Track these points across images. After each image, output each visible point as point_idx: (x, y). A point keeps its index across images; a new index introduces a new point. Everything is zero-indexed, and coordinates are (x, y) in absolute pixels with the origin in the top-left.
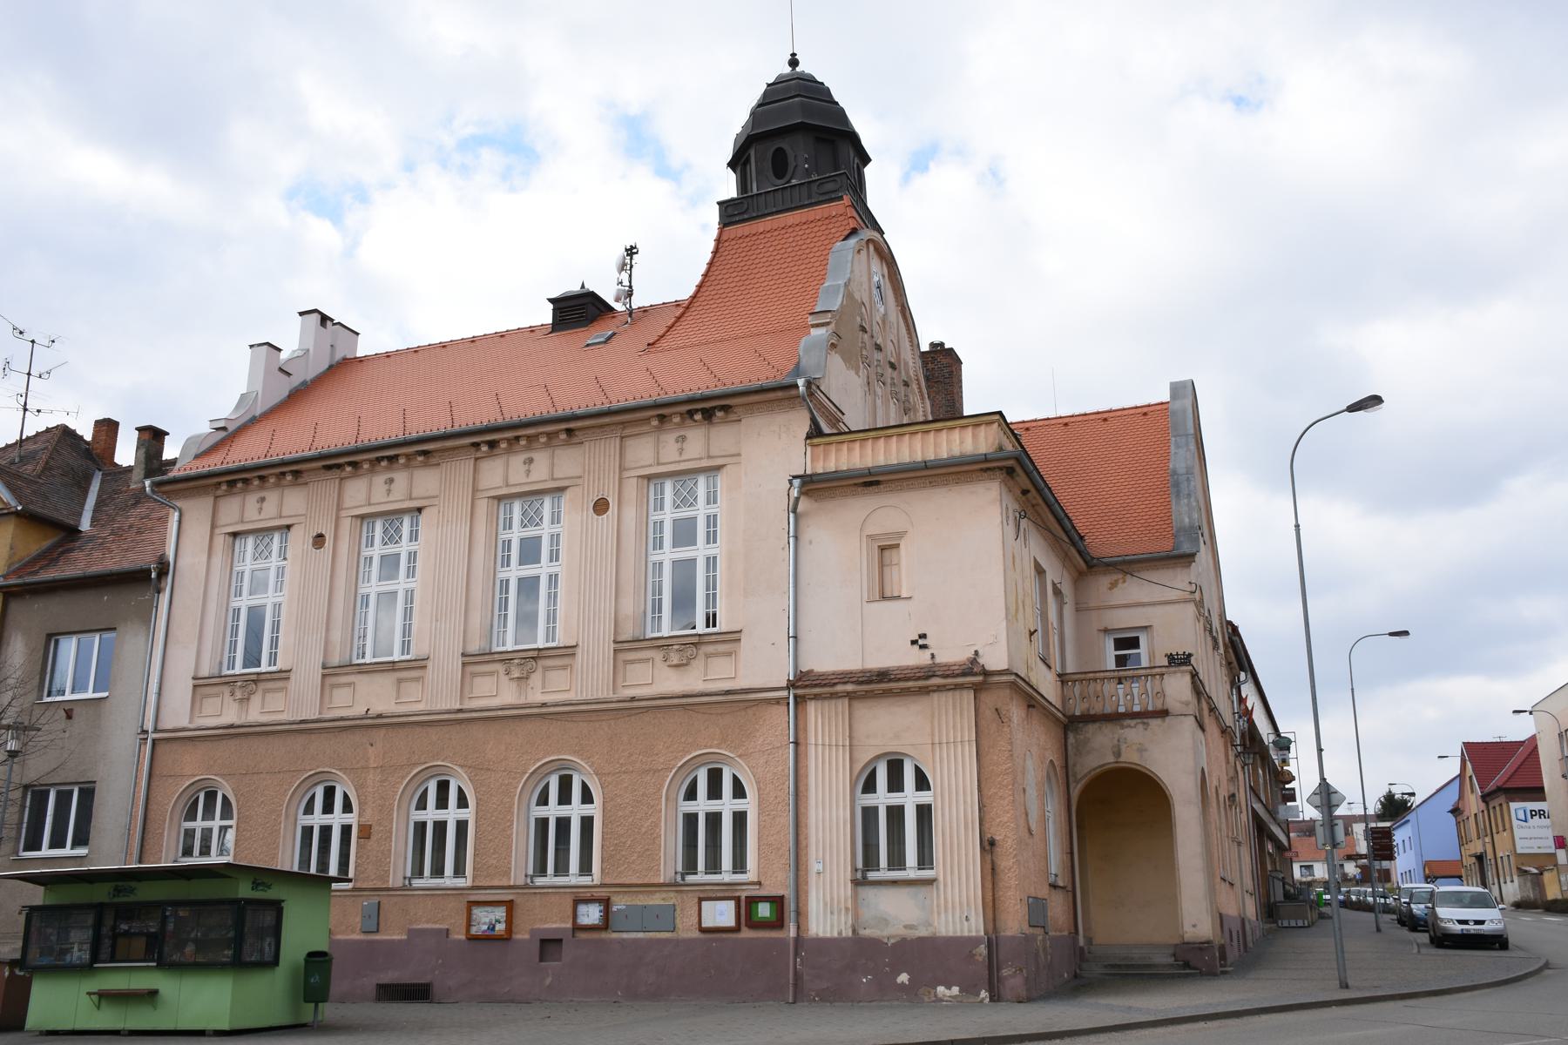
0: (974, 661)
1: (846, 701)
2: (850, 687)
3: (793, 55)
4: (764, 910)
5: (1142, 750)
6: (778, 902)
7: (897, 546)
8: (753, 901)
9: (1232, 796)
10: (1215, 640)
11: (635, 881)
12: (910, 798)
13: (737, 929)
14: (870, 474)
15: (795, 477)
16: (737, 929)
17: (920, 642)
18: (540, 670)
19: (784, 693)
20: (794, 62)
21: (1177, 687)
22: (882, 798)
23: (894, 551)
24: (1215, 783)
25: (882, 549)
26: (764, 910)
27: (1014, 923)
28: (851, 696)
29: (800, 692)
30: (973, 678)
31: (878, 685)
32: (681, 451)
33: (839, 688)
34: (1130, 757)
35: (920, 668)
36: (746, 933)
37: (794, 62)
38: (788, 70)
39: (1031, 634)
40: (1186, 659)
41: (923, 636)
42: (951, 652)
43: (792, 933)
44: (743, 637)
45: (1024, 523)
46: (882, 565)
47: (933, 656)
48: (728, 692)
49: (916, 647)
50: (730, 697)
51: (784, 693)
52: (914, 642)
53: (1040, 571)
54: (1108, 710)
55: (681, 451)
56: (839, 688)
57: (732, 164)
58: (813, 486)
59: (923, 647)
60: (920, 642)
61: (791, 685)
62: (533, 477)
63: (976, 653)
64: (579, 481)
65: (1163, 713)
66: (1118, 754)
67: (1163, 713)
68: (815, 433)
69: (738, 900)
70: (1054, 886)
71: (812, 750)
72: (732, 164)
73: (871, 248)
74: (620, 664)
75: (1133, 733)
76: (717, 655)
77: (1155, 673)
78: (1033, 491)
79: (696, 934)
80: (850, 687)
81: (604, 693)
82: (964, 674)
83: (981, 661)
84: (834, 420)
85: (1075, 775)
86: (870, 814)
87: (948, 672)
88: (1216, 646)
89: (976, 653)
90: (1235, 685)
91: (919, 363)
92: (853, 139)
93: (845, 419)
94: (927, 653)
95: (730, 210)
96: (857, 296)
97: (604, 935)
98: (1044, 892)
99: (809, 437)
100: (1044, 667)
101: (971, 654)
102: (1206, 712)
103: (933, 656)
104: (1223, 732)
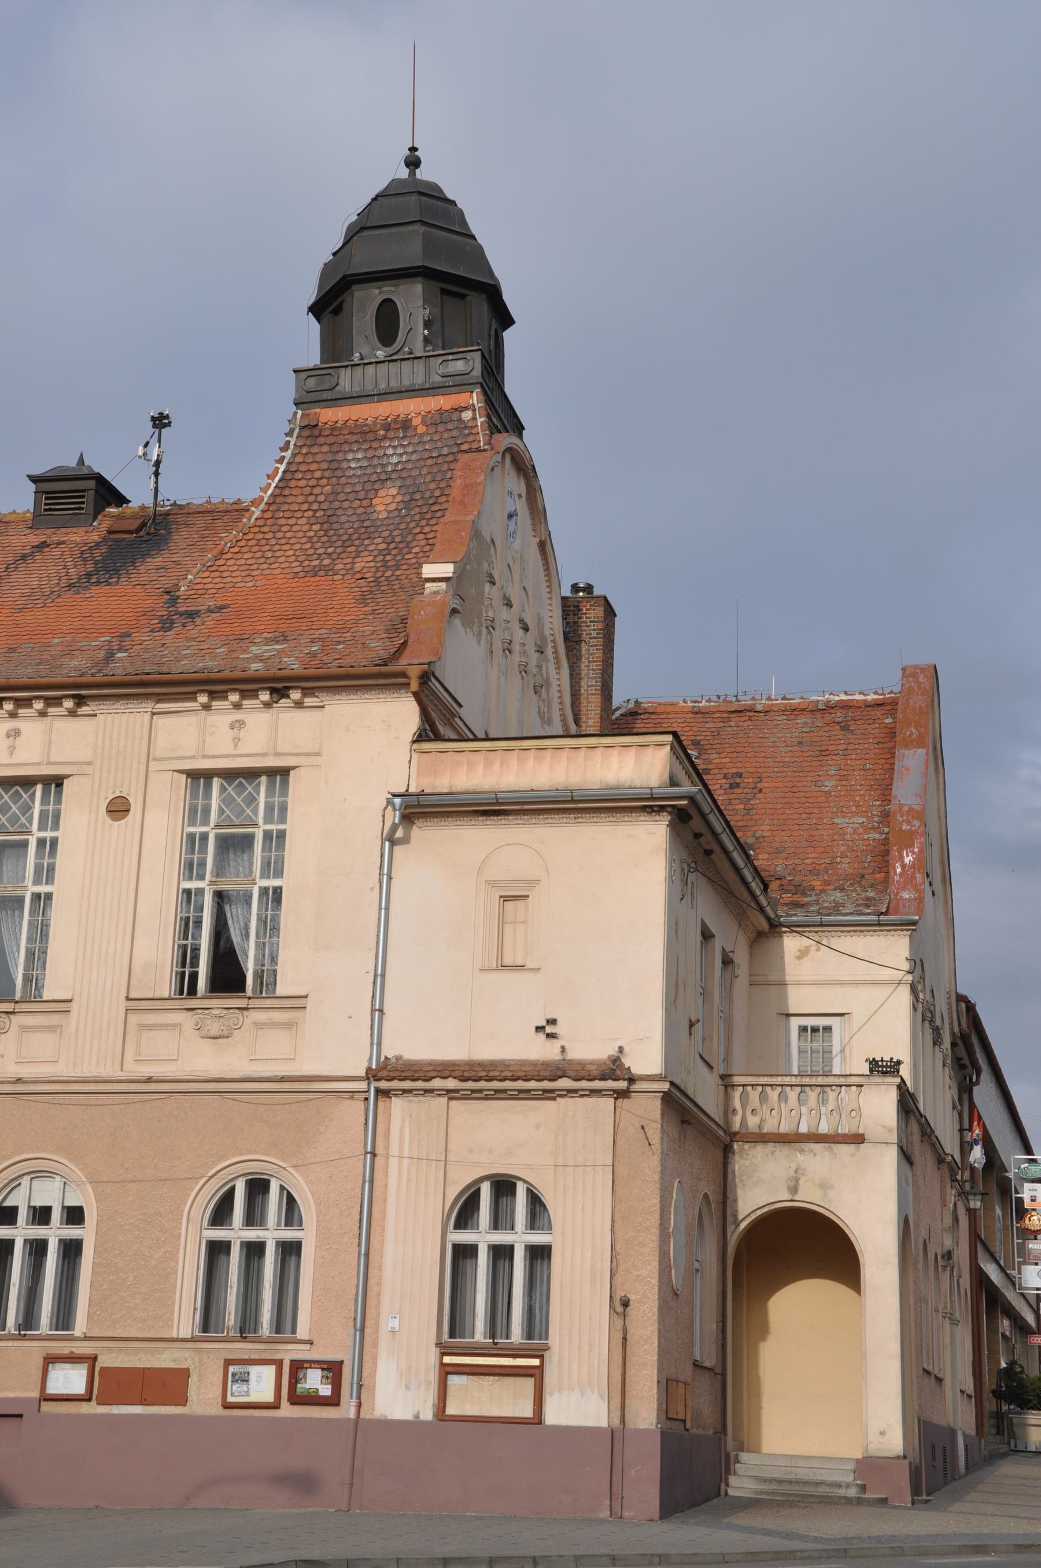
0: (616, 1060)
1: (445, 1100)
2: (451, 1083)
3: (413, 149)
4: (314, 1381)
5: (825, 1186)
6: (333, 1370)
7: (528, 896)
8: (298, 1367)
9: (948, 1255)
10: (937, 1031)
11: (133, 1334)
12: (272, 1233)
13: (275, 1406)
14: (498, 803)
15: (395, 796)
16: (275, 1406)
17: (547, 1029)
18: (14, 1030)
19: (362, 1086)
20: (413, 162)
21: (879, 1107)
22: (237, 1232)
23: (520, 904)
24: (923, 1234)
25: (506, 899)
26: (314, 1381)
27: (646, 1415)
28: (451, 1094)
29: (383, 1085)
30: (613, 1077)
31: (480, 1081)
32: (236, 741)
33: (437, 1083)
34: (809, 1197)
35: (546, 1064)
36: (287, 1410)
37: (413, 162)
38: (404, 173)
39: (691, 1025)
40: (891, 1068)
41: (552, 1022)
42: (588, 1047)
43: (352, 1415)
44: (309, 1003)
45: (692, 877)
46: (502, 922)
47: (563, 1049)
48: (283, 1079)
49: (542, 1036)
50: (287, 1086)
51: (362, 1086)
52: (539, 1029)
53: (707, 935)
54: (784, 1129)
55: (236, 741)
56: (437, 1083)
57: (317, 309)
58: (416, 810)
59: (551, 1036)
60: (547, 1029)
61: (371, 1075)
62: (19, 757)
63: (621, 1049)
64: (88, 769)
65: (858, 1139)
66: (794, 1190)
67: (858, 1139)
68: (428, 732)
69: (279, 1364)
70: (696, 1365)
71: (393, 1163)
72: (317, 309)
73: (508, 458)
74: (132, 1030)
75: (816, 1162)
76: (272, 1025)
77: (847, 1082)
78: (708, 836)
79: (218, 1411)
80: (451, 1083)
81: (108, 1069)
82: (603, 1078)
83: (627, 1062)
84: (450, 716)
85: (735, 1215)
86: (464, 1253)
87: (581, 1071)
88: (937, 1041)
89: (621, 1049)
90: (965, 1090)
91: (558, 612)
92: (492, 293)
93: (462, 712)
94: (556, 1045)
95: (311, 383)
96: (486, 535)
97: (85, 1408)
98: (686, 1372)
99: (420, 738)
100: (704, 1069)
101: (613, 1051)
102: (916, 1137)
103: (563, 1049)
104: (940, 1161)
